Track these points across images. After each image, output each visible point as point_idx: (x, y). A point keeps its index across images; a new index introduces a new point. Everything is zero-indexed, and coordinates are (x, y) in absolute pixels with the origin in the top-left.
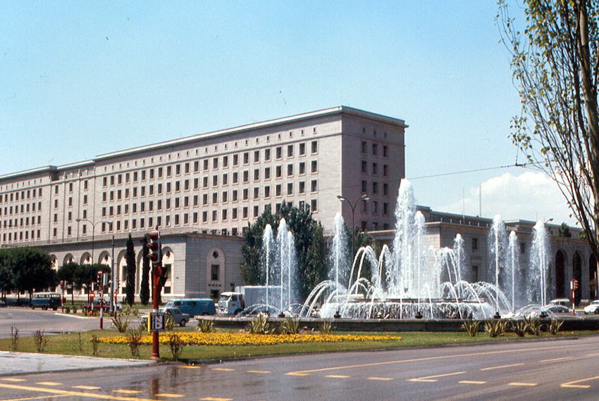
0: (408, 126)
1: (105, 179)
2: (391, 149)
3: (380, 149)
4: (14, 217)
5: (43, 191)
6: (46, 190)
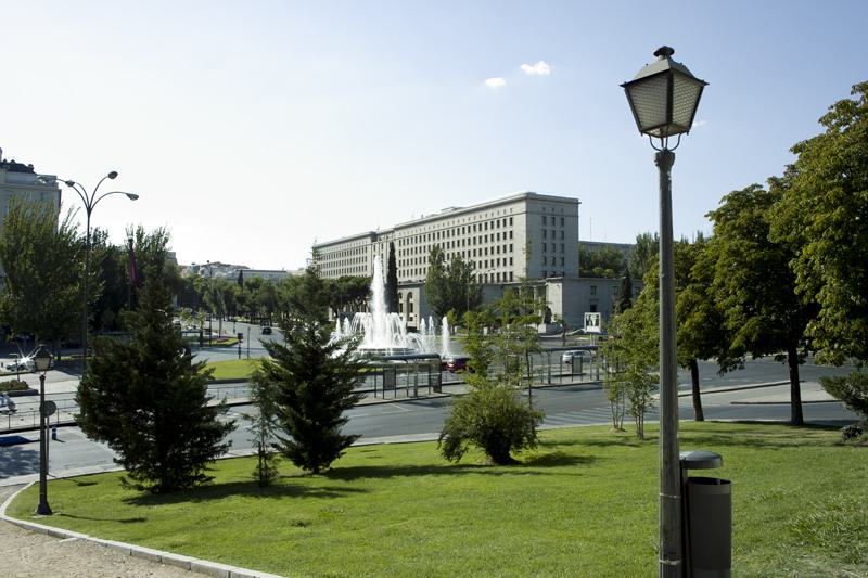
2: (567, 220)
3: (558, 219)
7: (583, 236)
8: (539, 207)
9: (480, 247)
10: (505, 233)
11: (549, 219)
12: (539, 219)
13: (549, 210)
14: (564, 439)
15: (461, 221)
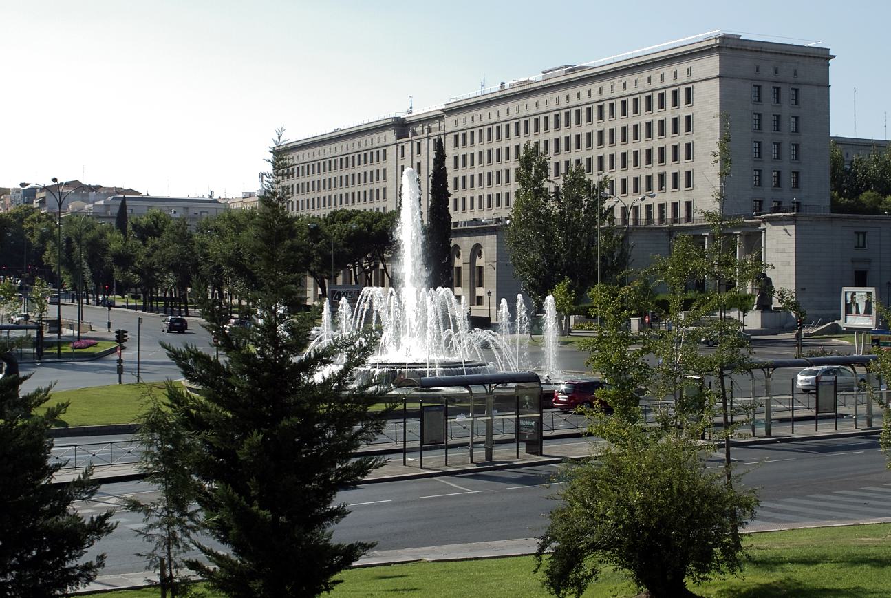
0: (834, 57)
1: (456, 137)
2: (805, 92)
3: (786, 93)
4: (656, 116)
5: (387, 153)
6: (391, 151)
12: (747, 89)
13: (767, 72)
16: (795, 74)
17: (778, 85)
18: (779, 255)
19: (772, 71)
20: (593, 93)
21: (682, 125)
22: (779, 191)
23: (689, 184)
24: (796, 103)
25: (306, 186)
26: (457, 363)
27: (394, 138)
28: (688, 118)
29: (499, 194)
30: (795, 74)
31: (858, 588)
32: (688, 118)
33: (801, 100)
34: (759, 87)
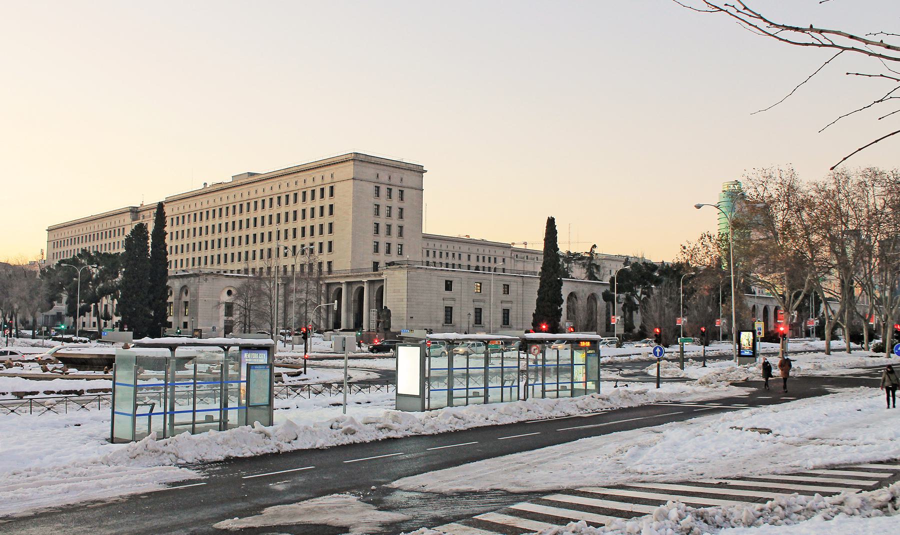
3: (395, 193)
4: (259, 214)
5: (125, 230)
7: (429, 228)
8: (370, 172)
9: (67, 249)
10: (322, 208)
11: (383, 191)
13: (384, 178)
14: (321, 455)
15: (117, 222)
16: (401, 180)
17: (390, 187)
18: (396, 294)
19: (387, 178)
20: (266, 190)
21: (326, 211)
22: (389, 256)
23: (330, 250)
24: (402, 200)
25: (62, 253)
26: (646, 382)
27: (131, 220)
28: (331, 206)
29: (200, 257)
30: (401, 180)
31: (185, 480)
32: (331, 206)
33: (405, 197)
34: (378, 187)
